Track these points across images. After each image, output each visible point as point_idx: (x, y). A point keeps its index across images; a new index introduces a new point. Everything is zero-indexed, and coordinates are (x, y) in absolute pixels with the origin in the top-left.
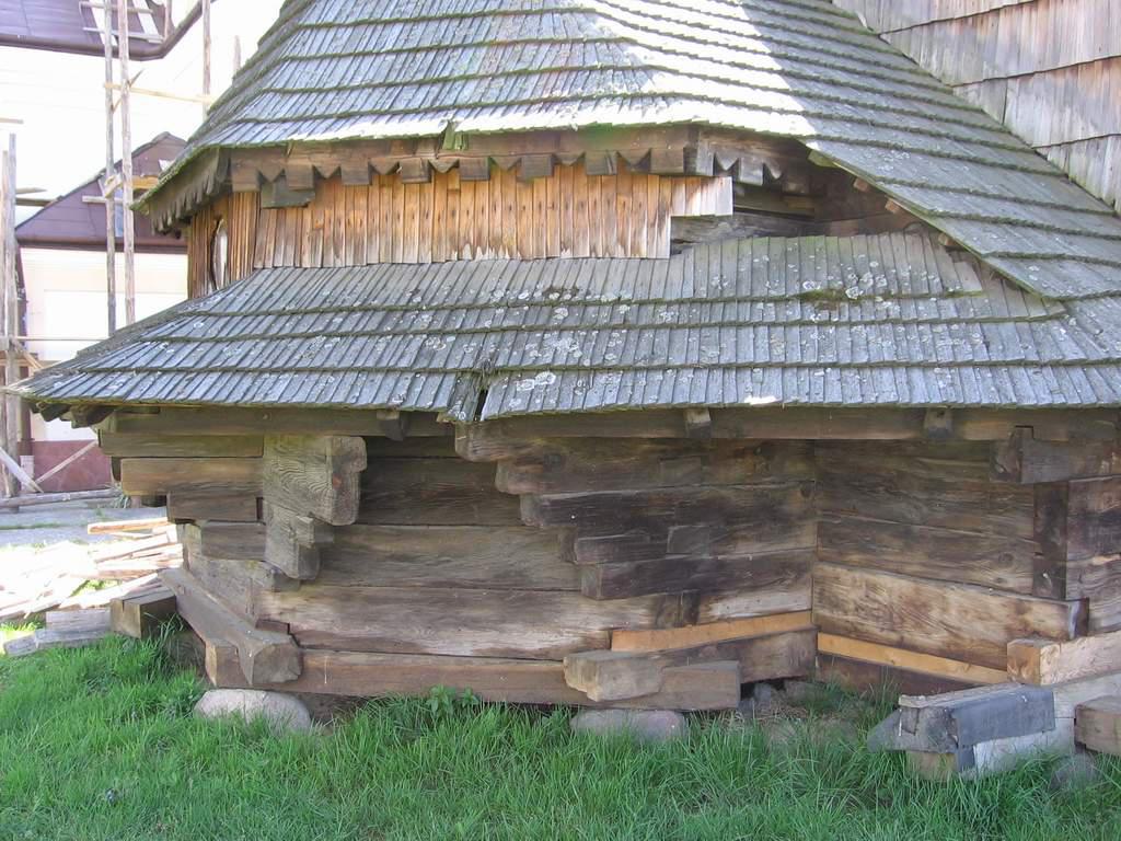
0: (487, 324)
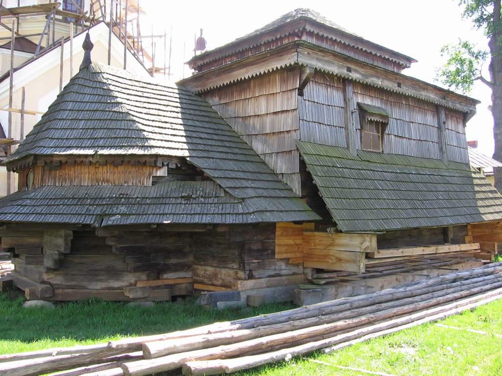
0: (104, 203)
